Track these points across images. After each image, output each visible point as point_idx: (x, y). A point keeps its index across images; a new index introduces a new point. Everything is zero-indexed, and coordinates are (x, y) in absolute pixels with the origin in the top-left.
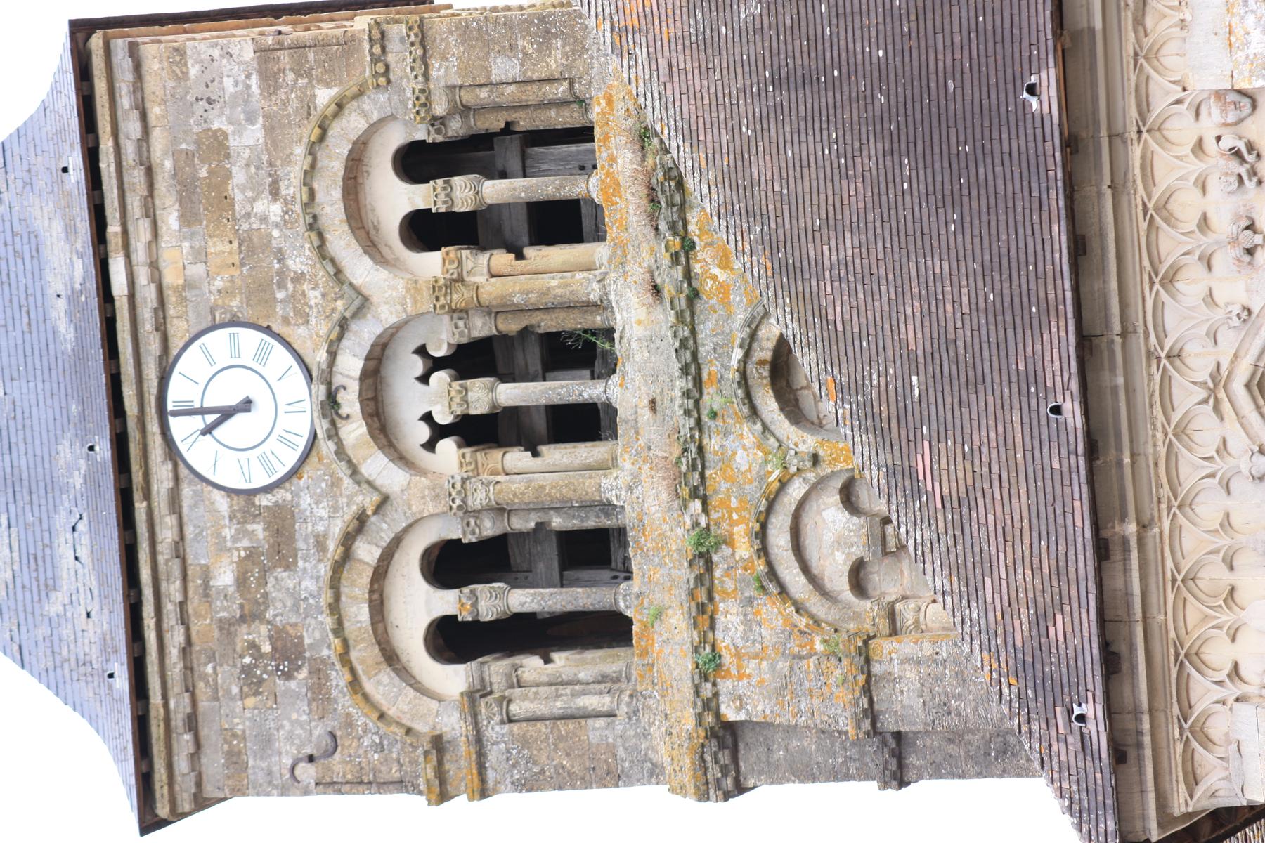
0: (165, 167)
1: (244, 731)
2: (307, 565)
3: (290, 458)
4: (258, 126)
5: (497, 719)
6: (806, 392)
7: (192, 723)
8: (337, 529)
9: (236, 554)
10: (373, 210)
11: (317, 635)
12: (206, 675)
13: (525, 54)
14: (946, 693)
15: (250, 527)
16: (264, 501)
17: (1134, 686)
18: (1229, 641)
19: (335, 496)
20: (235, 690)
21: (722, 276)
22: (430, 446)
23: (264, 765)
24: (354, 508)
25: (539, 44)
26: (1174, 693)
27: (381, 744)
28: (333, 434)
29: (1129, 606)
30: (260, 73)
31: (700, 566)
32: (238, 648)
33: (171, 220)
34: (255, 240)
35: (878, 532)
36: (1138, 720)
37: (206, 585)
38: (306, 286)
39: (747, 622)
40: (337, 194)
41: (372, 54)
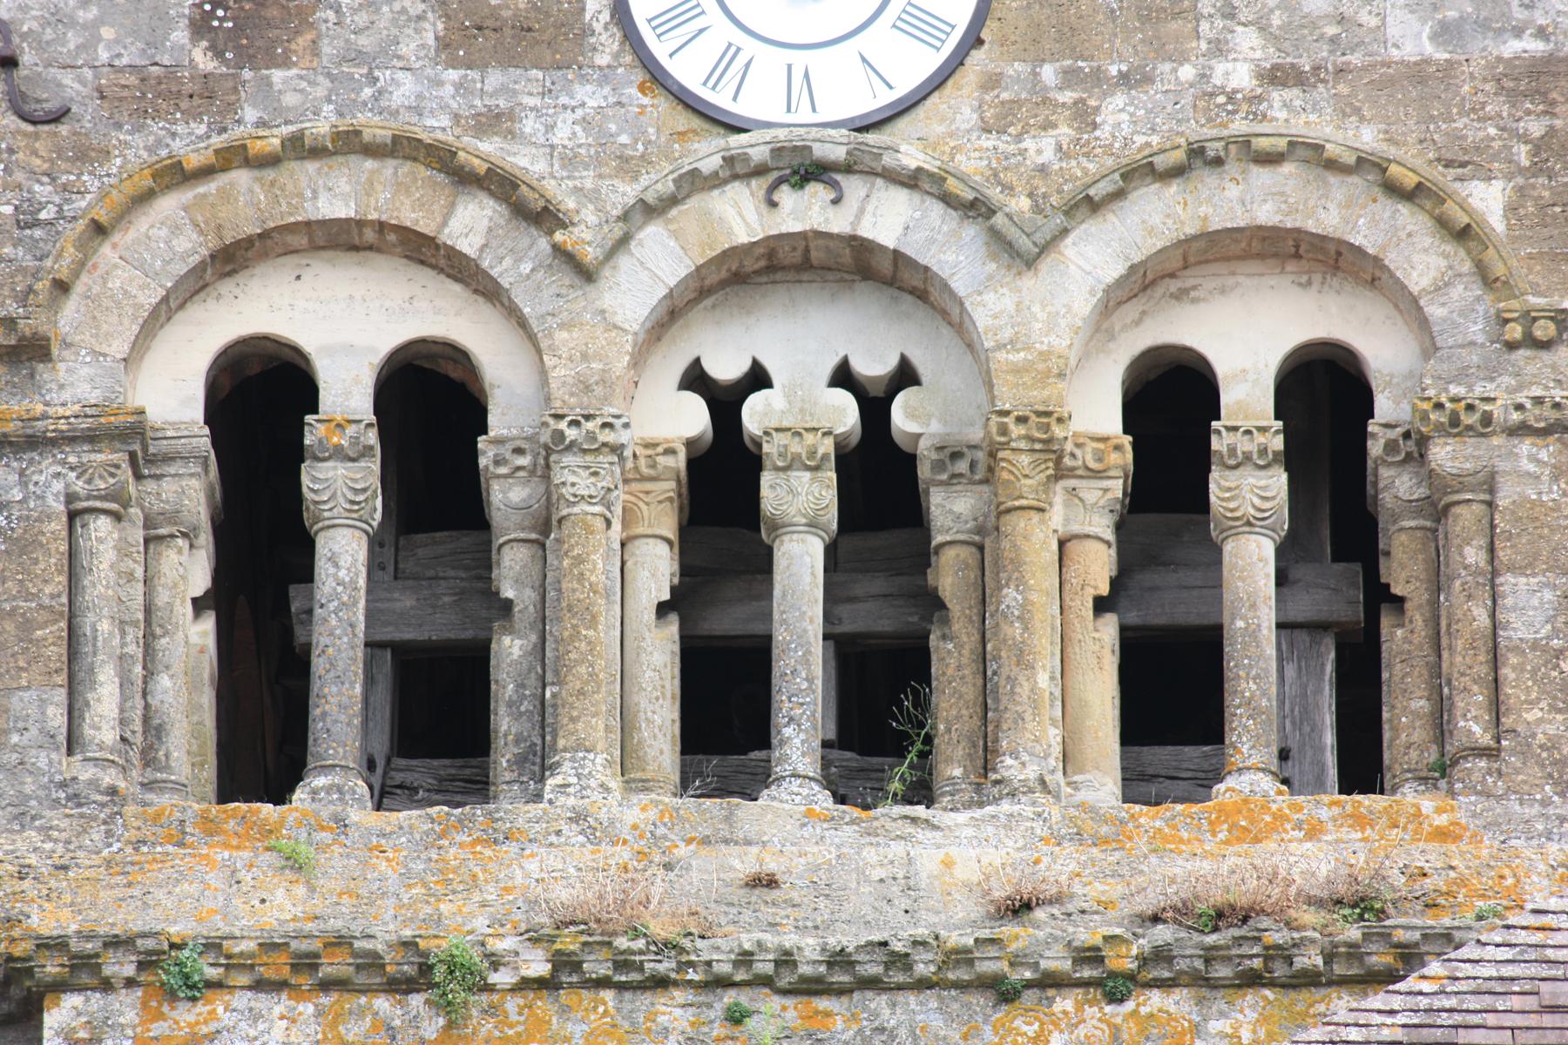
2: (449, 89)
3: (688, 71)
4: (1429, 49)
8: (525, 161)
10: (1223, 291)
19: (598, 161)
22: (695, 379)
24: (570, 204)
27: (36, 223)
28: (737, 170)
34: (1174, 26)
38: (1065, 131)
40: (1266, 214)
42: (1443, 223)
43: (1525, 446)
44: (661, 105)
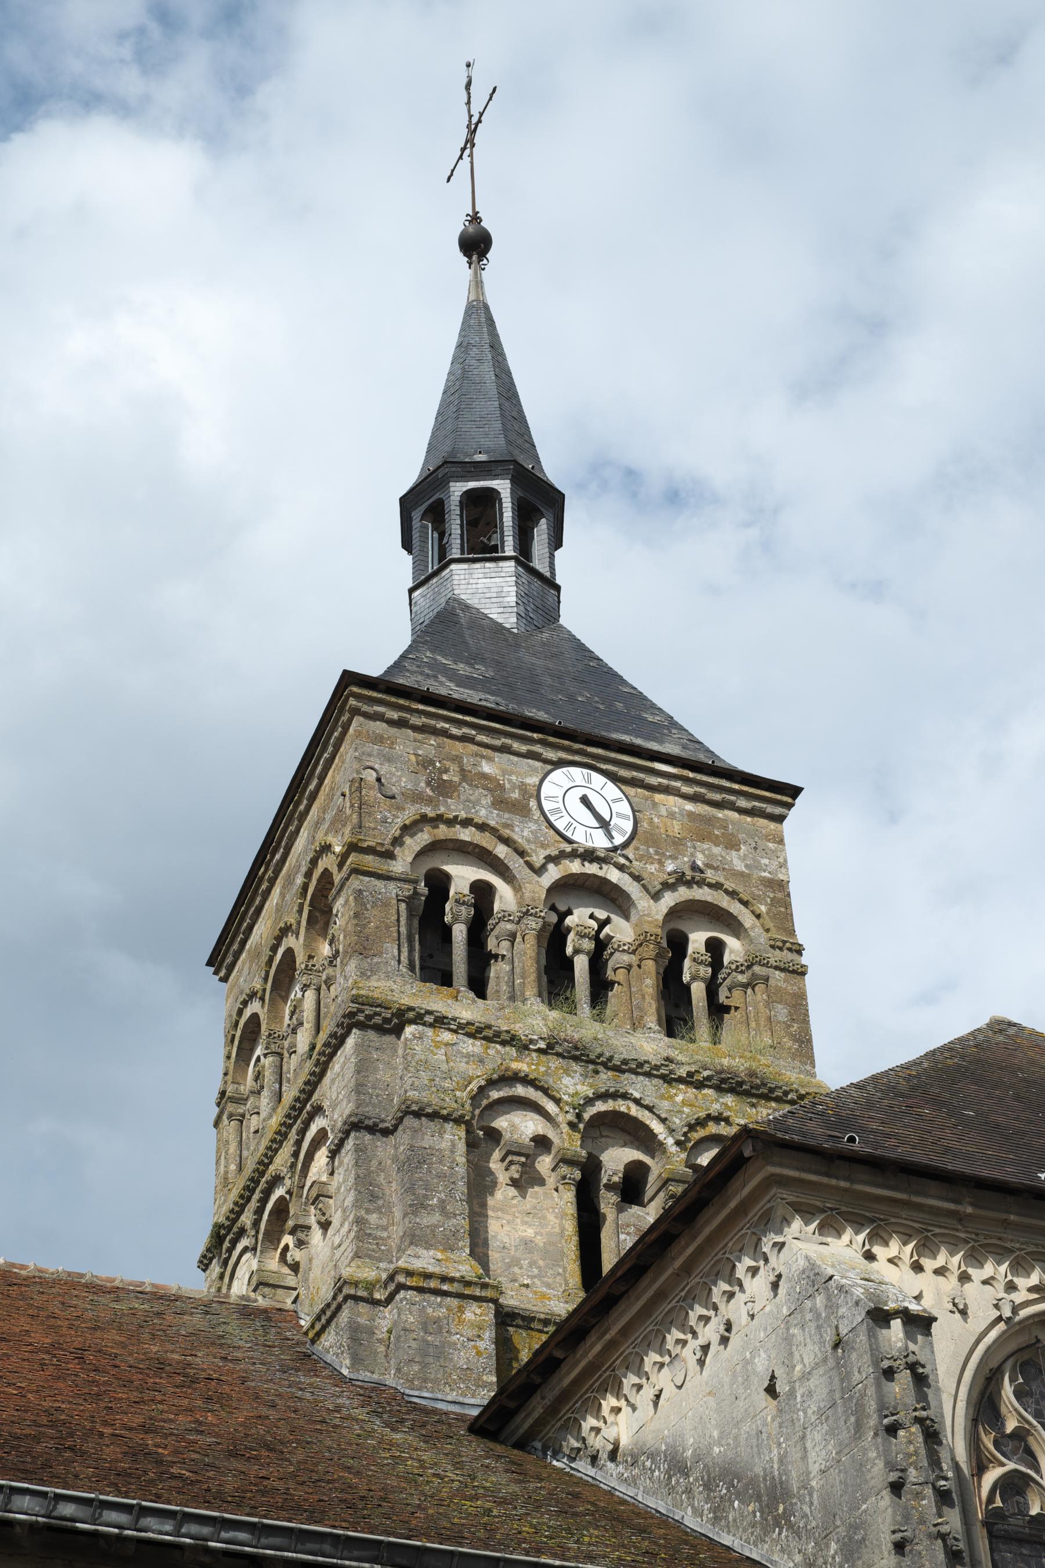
0: (720, 814)
1: (395, 749)
2: (495, 815)
3: (560, 825)
4: (744, 869)
5: (400, 893)
6: (598, 1133)
7: (401, 724)
9: (502, 778)
10: (690, 919)
11: (452, 807)
12: (430, 740)
13: (789, 1026)
14: (432, 1164)
15: (517, 791)
16: (533, 803)
17: (866, 1183)
18: (890, 1256)
19: (535, 843)
20: (420, 752)
21: (679, 1098)
23: (375, 753)
24: (529, 851)
25: (795, 1035)
26: (855, 1211)
27: (386, 822)
29: (917, 1193)
30: (772, 879)
31: (505, 1037)
32: (445, 762)
33: (689, 807)
34: (682, 847)
35: (524, 1151)
36: (846, 1179)
37: (483, 757)
38: (657, 865)
39: (468, 1055)
41: (787, 942)
42: (753, 912)
43: (777, 972)
44: (552, 832)
